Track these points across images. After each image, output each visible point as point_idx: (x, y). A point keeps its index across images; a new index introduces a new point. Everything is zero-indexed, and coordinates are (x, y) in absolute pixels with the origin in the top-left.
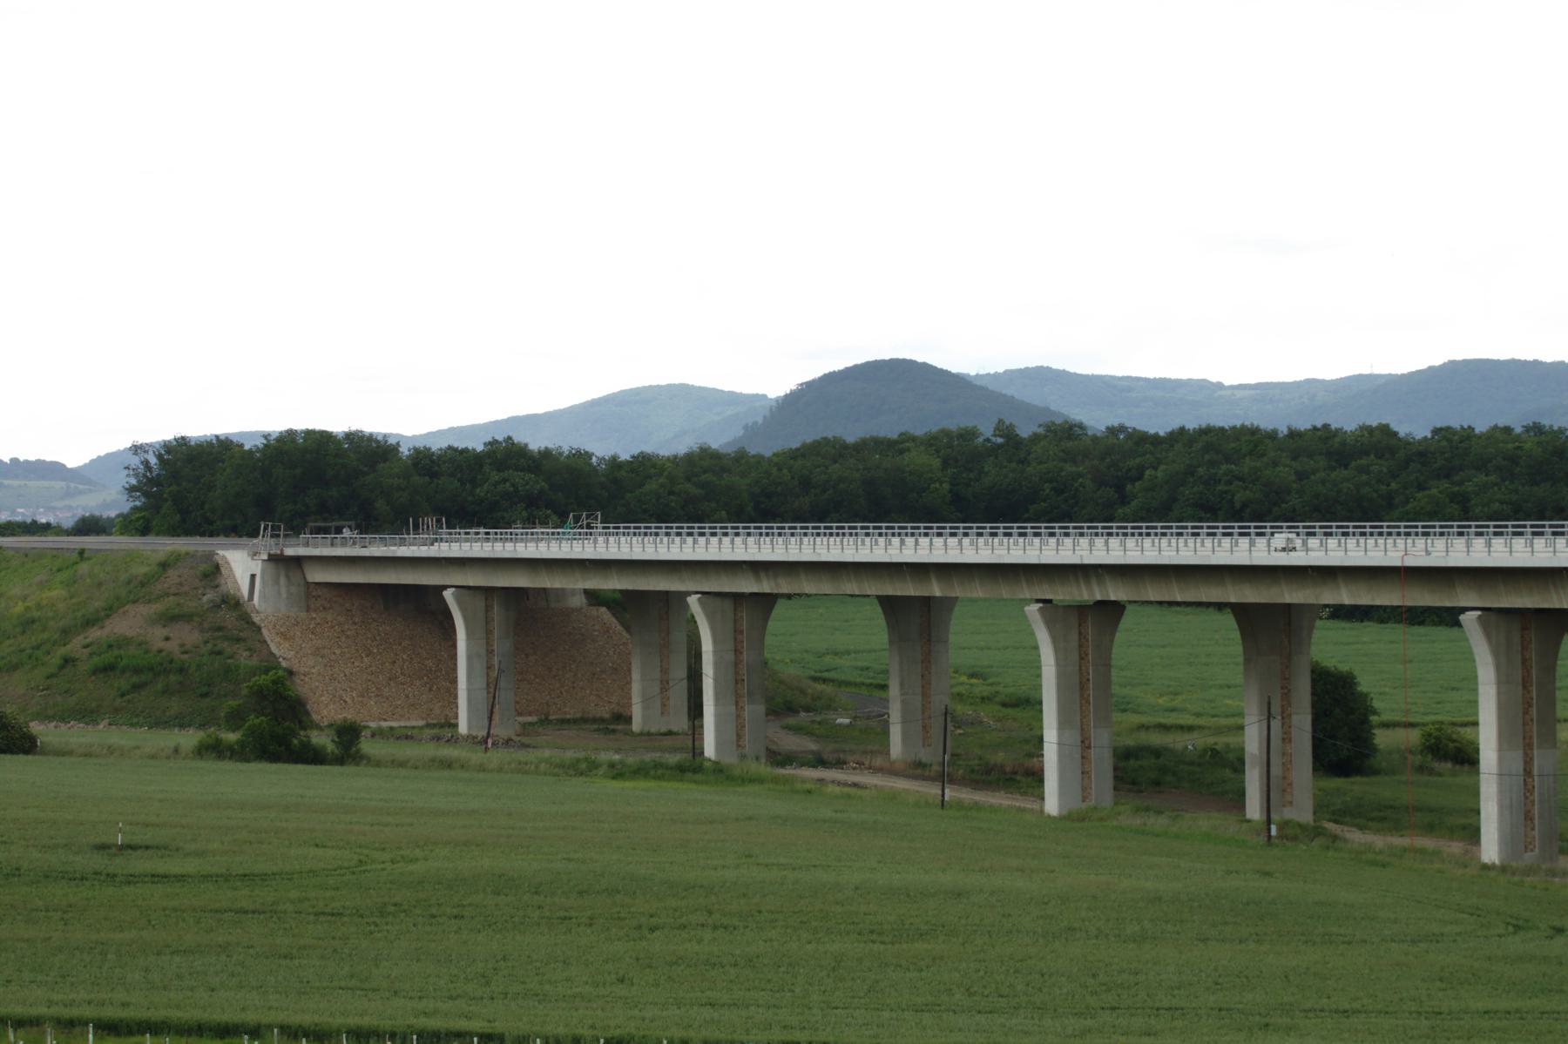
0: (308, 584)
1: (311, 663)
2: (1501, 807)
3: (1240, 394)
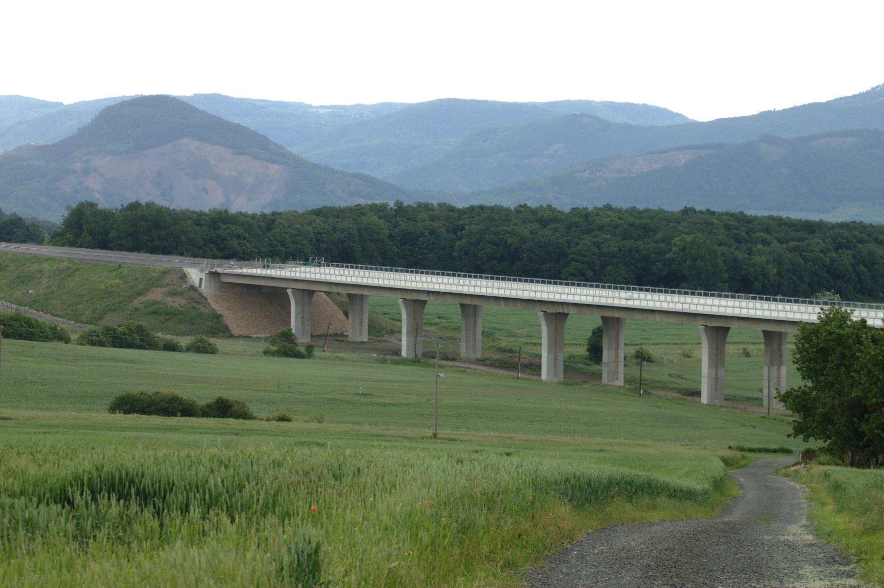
0: (221, 282)
1: (227, 312)
2: (708, 386)
3: (321, 111)
